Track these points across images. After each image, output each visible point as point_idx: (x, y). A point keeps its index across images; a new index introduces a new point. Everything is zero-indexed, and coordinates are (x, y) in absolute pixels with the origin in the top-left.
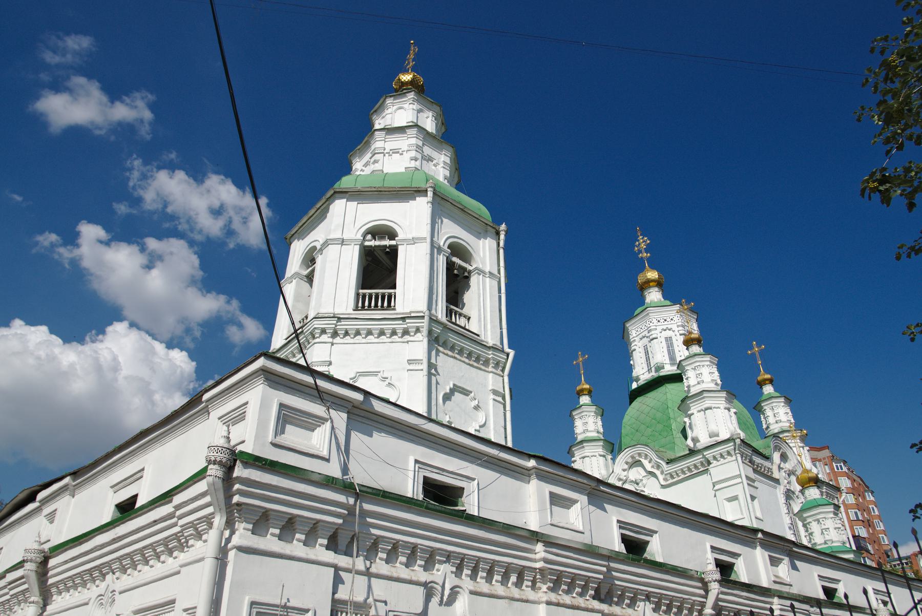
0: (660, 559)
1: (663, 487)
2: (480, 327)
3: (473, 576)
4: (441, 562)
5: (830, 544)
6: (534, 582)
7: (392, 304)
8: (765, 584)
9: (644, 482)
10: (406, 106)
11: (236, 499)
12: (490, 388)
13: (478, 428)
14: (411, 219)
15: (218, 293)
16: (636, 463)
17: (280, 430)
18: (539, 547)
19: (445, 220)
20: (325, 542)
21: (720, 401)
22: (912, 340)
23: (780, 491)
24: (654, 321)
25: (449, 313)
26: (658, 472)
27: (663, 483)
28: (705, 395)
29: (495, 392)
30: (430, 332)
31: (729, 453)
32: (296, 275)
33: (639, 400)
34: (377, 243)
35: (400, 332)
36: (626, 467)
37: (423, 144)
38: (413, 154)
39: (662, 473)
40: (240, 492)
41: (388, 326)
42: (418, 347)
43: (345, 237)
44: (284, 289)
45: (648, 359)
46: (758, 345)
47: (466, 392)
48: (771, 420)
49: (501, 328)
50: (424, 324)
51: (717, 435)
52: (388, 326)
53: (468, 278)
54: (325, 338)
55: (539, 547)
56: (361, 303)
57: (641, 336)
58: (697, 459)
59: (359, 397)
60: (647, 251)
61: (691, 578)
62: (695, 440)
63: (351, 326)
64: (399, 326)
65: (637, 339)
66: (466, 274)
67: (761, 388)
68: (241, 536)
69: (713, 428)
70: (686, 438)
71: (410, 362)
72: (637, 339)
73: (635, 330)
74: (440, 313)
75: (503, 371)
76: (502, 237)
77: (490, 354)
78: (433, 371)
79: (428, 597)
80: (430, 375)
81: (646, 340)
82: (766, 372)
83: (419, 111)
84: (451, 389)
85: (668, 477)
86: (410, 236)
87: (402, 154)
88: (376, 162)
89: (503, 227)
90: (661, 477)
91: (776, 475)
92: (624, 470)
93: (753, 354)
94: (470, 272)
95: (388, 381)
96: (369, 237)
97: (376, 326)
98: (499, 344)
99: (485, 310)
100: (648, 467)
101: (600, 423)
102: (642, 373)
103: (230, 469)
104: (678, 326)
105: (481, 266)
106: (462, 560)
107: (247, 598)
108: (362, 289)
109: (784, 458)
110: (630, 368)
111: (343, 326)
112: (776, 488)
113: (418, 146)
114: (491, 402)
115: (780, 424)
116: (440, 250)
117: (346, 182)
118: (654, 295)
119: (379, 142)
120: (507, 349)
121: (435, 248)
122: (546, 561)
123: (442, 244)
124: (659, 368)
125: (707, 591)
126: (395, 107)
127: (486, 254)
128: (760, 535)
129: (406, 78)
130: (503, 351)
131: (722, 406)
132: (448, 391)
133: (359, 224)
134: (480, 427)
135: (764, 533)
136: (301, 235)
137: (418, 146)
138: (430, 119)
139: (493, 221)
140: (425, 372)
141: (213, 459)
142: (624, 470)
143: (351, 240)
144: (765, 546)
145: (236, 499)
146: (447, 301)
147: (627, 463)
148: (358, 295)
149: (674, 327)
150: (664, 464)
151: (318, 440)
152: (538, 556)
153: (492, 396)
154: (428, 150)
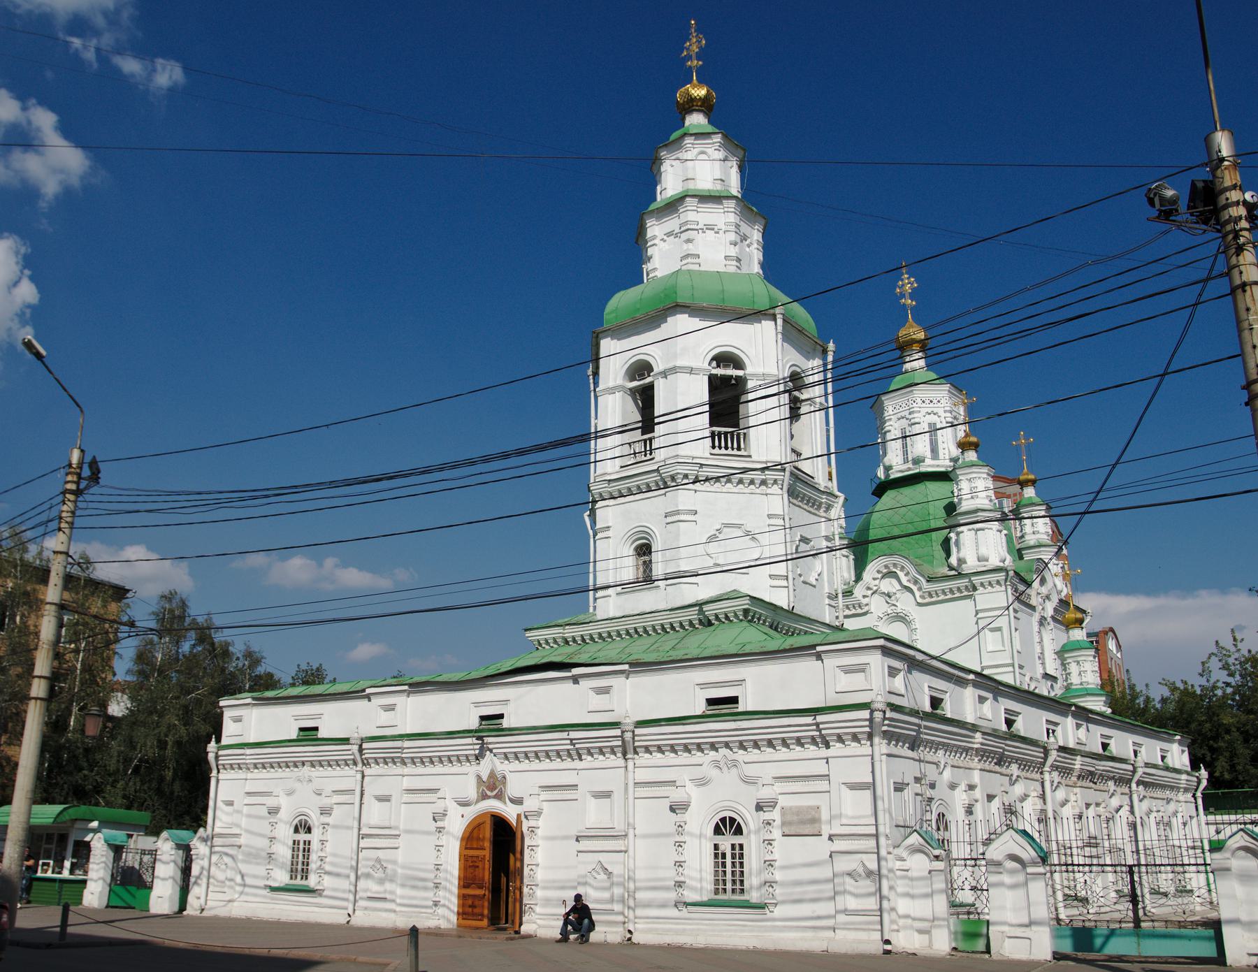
0: (1022, 734)
1: (919, 604)
5: (1085, 686)
8: (1071, 746)
10: (710, 151)
16: (891, 574)
18: (978, 735)
21: (725, 216)
23: (1036, 617)
24: (919, 401)
26: (914, 588)
27: (920, 600)
31: (998, 582)
35: (758, 482)
39: (920, 589)
46: (1026, 438)
55: (978, 735)
58: (963, 582)
61: (1038, 746)
69: (983, 551)
70: (948, 554)
73: (892, 407)
82: (1031, 471)
85: (926, 595)
89: (831, 346)
91: (1033, 602)
93: (1018, 446)
109: (1043, 581)
112: (1031, 615)
115: (1038, 536)
118: (916, 363)
124: (917, 461)
125: (1045, 758)
126: (696, 151)
135: (1076, 706)
139: (820, 337)
144: (1075, 716)
150: (923, 581)
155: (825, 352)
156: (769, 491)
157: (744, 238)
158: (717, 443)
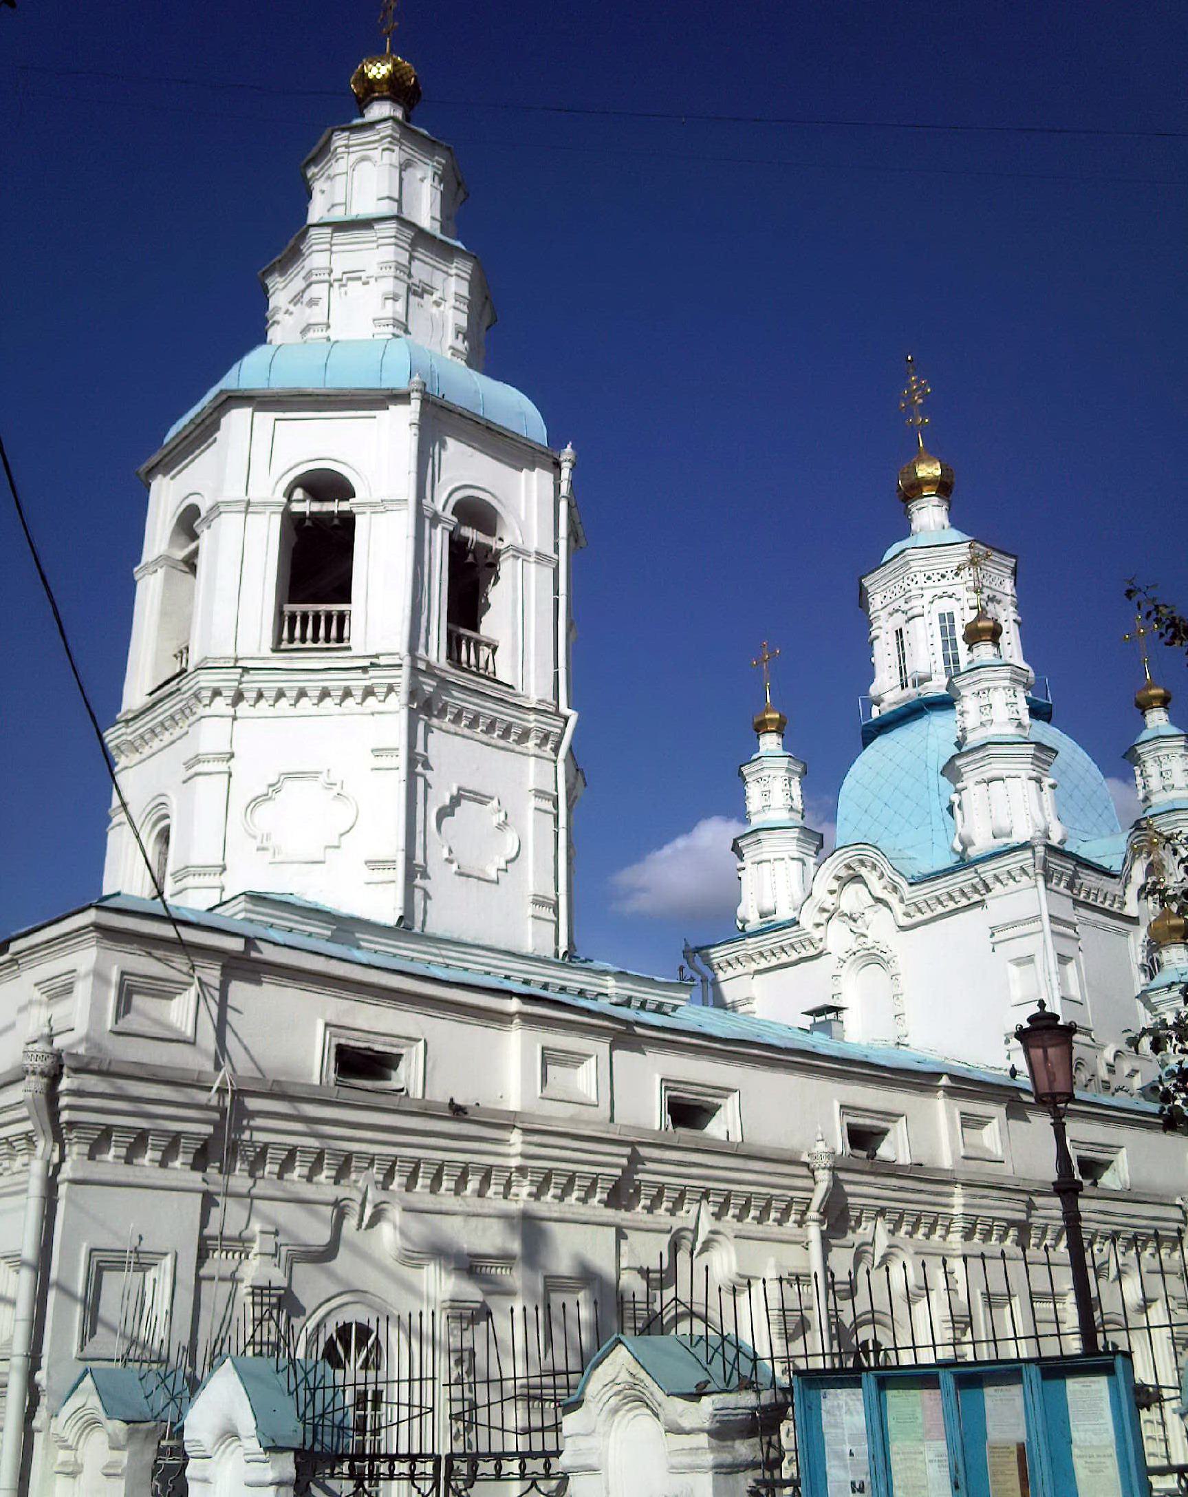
1: (902, 928)
2: (514, 668)
3: (410, 1186)
4: (360, 1170)
6: (508, 1185)
7: (346, 634)
9: (868, 917)
10: (376, 154)
11: (65, 1116)
12: (532, 786)
13: (503, 866)
14: (376, 455)
15: (323, 153)
17: (124, 1006)
18: (516, 1137)
19: (450, 442)
20: (190, 1159)
25: (454, 643)
26: (892, 899)
27: (905, 921)
28: (993, 750)
29: (540, 794)
30: (413, 694)
31: (1024, 871)
32: (164, 560)
33: (880, 743)
34: (316, 507)
35: (358, 693)
36: (835, 885)
37: (412, 258)
38: (388, 285)
39: (902, 900)
40: (69, 1107)
41: (335, 682)
42: (389, 721)
43: (254, 496)
44: (118, 778)
45: (902, 658)
47: (481, 799)
48: (1154, 783)
49: (556, 666)
50: (402, 678)
51: (1009, 834)
52: (335, 682)
53: (493, 566)
54: (221, 705)
55: (516, 1137)
56: (288, 631)
57: (890, 609)
58: (963, 879)
59: (237, 945)
60: (924, 409)
62: (966, 843)
63: (270, 683)
64: (358, 682)
66: (490, 560)
67: (1143, 714)
68: (73, 1169)
71: (377, 752)
73: (881, 592)
74: (436, 651)
75: (556, 750)
76: (566, 473)
77: (532, 721)
78: (419, 769)
79: (341, 1216)
80: (412, 777)
81: (899, 619)
83: (405, 166)
84: (452, 798)
85: (912, 910)
86: (376, 497)
87: (366, 283)
88: (313, 302)
89: (567, 453)
90: (899, 908)
92: (832, 892)
94: (498, 553)
95: (337, 789)
96: (299, 493)
98: (550, 698)
99: (525, 621)
100: (878, 888)
101: (796, 790)
102: (887, 689)
103: (54, 1077)
105: (519, 542)
107: (85, 1245)
108: (290, 602)
110: (869, 674)
111: (251, 684)
113: (399, 266)
114: (530, 813)
116: (436, 519)
117: (250, 372)
118: (930, 515)
119: (320, 254)
120: (564, 709)
121: (424, 519)
122: (524, 1156)
123: (439, 508)
126: (353, 157)
127: (530, 508)
128: (944, 1081)
129: (379, 71)
130: (557, 713)
131: (1023, 774)
132: (447, 802)
133: (280, 465)
134: (507, 862)
136: (171, 462)
137: (399, 266)
138: (428, 182)
140: (402, 773)
141: (31, 1069)
142: (832, 892)
143: (266, 504)
144: (951, 1092)
146: (450, 619)
147: (838, 878)
148: (280, 613)
149: (960, 590)
150: (904, 884)
151: (180, 1011)
152: (512, 1150)
153: (533, 802)
154: (421, 271)
155: (557, 465)
156: (381, 707)
157: (417, 291)
158: (322, 633)
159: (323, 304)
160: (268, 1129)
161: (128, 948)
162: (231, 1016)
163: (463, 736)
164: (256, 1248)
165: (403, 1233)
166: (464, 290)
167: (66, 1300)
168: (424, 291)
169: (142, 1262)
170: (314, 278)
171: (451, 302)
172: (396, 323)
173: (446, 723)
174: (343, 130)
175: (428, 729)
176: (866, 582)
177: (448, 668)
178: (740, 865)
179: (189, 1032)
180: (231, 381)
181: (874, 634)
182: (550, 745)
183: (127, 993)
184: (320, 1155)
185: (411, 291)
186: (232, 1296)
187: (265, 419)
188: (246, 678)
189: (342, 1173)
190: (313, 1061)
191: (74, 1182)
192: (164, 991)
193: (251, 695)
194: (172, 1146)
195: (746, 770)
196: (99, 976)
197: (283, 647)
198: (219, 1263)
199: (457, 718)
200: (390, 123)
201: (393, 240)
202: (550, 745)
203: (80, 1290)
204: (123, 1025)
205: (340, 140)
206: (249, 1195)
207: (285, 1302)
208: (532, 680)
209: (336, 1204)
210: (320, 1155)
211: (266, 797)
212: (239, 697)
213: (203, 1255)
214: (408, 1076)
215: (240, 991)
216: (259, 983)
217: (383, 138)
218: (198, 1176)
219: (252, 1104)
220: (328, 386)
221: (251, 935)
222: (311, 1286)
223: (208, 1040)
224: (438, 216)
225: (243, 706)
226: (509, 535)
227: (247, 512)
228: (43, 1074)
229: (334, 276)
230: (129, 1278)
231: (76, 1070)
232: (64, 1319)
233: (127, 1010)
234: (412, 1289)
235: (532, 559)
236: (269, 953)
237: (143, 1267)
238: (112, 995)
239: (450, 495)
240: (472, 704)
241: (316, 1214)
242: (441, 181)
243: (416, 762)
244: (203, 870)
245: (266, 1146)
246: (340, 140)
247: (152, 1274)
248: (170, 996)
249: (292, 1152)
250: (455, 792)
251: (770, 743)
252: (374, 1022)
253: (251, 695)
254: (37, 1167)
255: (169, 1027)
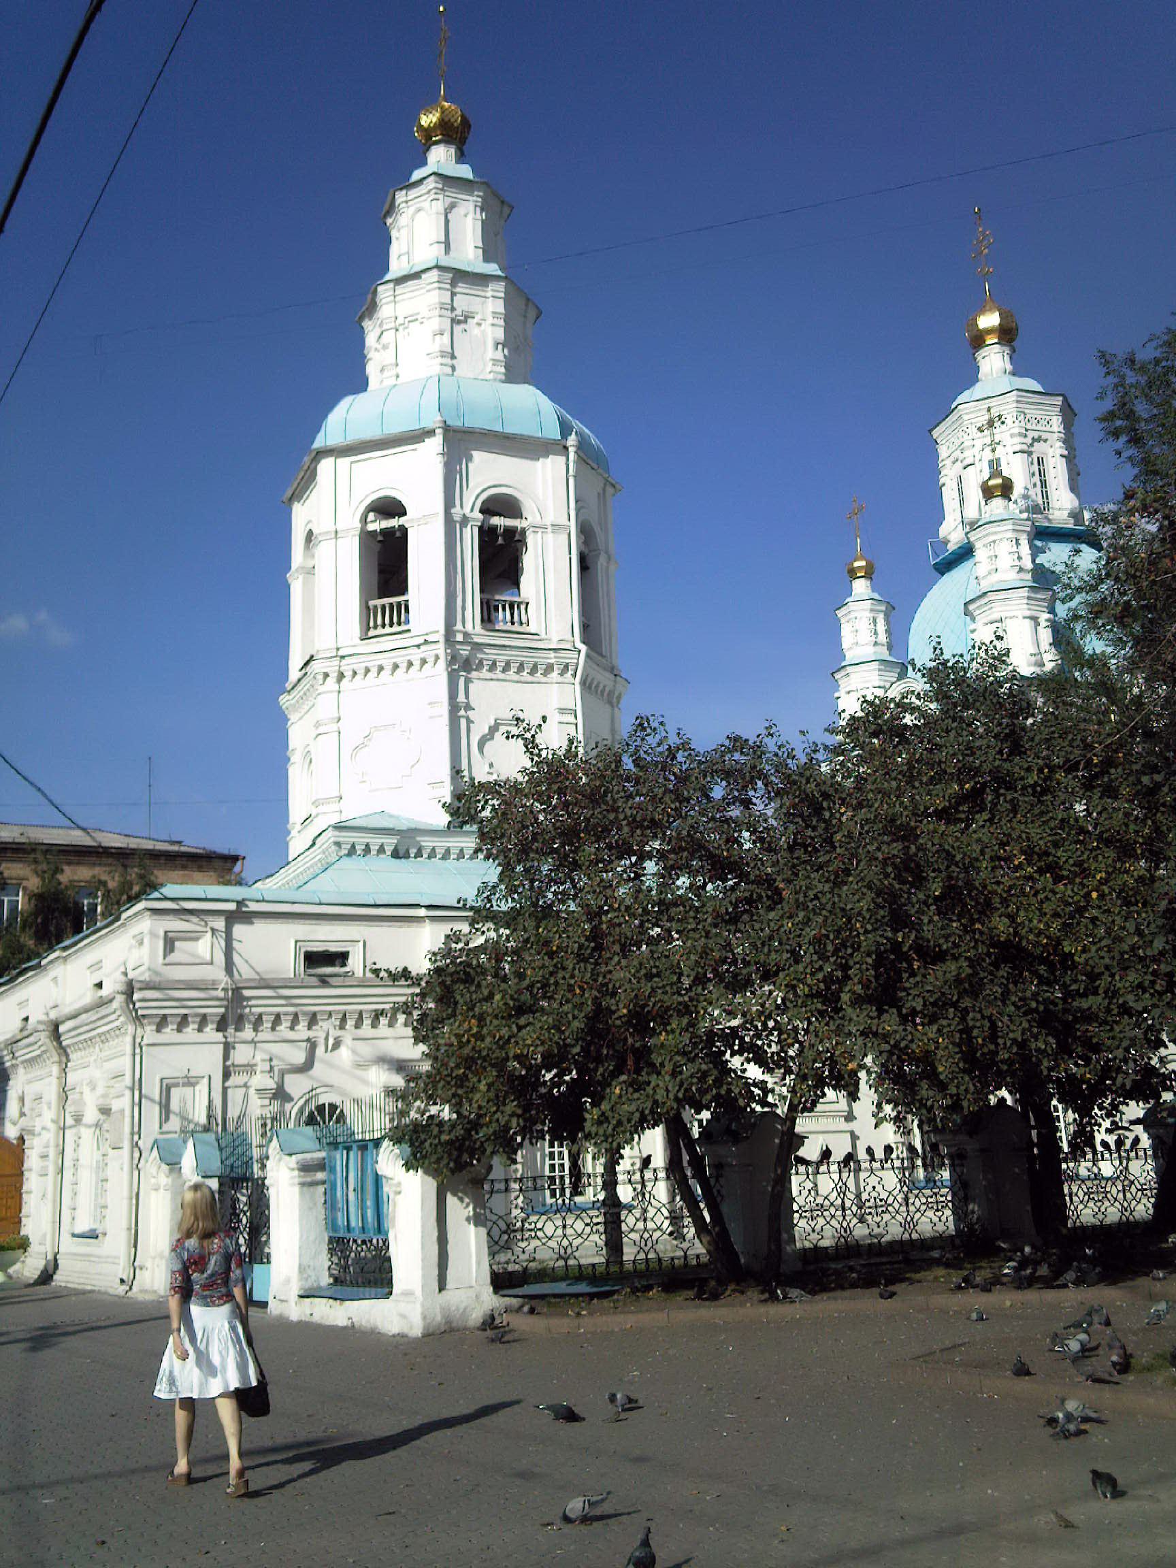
11: (140, 1012)
15: (391, 209)
20: (215, 1026)
22: (801, 732)
28: (992, 596)
37: (453, 294)
40: (140, 1001)
41: (401, 658)
52: (401, 658)
53: (523, 541)
57: (952, 459)
59: (232, 906)
65: (948, 462)
72: (948, 462)
76: (572, 455)
77: (552, 658)
94: (523, 531)
96: (371, 516)
97: (387, 660)
98: (569, 637)
101: (881, 627)
104: (1012, 436)
106: (345, 1015)
116: (465, 521)
123: (467, 510)
126: (412, 210)
127: (546, 493)
129: (428, 119)
145: (140, 1012)
155: (566, 448)
159: (392, 347)
160: (260, 1003)
161: (168, 917)
162: (235, 944)
163: (498, 680)
164: (259, 1069)
165: (354, 1052)
166: (500, 307)
167: (149, 1103)
168: (466, 317)
169: (190, 1082)
170: (385, 327)
171: (490, 320)
172: (443, 354)
173: (485, 673)
174: (401, 189)
175: (468, 681)
176: (935, 433)
177: (483, 632)
178: (972, 627)
179: (208, 958)
180: (318, 443)
181: (941, 482)
182: (570, 672)
183: (170, 944)
184: (296, 1015)
185: (454, 321)
186: (246, 1096)
187: (344, 462)
188: (344, 662)
189: (313, 1020)
190: (287, 963)
191: (148, 1045)
192: (193, 937)
193: (348, 674)
194: (203, 1021)
195: (840, 613)
196: (153, 935)
197: (371, 633)
198: (234, 1080)
199: (493, 667)
200: (433, 177)
201: (436, 285)
202: (570, 672)
203: (157, 1098)
204: (167, 961)
205: (401, 197)
206: (253, 1041)
207: (280, 1094)
208: (553, 627)
209: (308, 1040)
210: (296, 1015)
211: (364, 745)
212: (341, 676)
213: (226, 1075)
214: (355, 964)
215: (239, 930)
216: (252, 923)
217: (429, 191)
218: (220, 1034)
219: (247, 993)
220: (386, 432)
221: (240, 899)
222: (297, 1086)
223: (220, 958)
224: (480, 245)
225: (345, 681)
226: (530, 517)
227: (336, 538)
228: (123, 993)
229: (398, 322)
230: (188, 1091)
231: (141, 989)
232: (152, 1113)
233: (172, 950)
234: (366, 1082)
235: (549, 530)
236: (253, 907)
237: (193, 1085)
238: (161, 944)
239: (483, 491)
240: (501, 657)
241: (300, 1048)
242: (482, 210)
243: (457, 710)
244: (327, 801)
245: (260, 1015)
246: (401, 197)
247: (197, 1088)
248: (197, 939)
249: (278, 1016)
250: (492, 723)
251: (861, 587)
252: (326, 936)
253: (348, 674)
254: (129, 1039)
255: (199, 957)
